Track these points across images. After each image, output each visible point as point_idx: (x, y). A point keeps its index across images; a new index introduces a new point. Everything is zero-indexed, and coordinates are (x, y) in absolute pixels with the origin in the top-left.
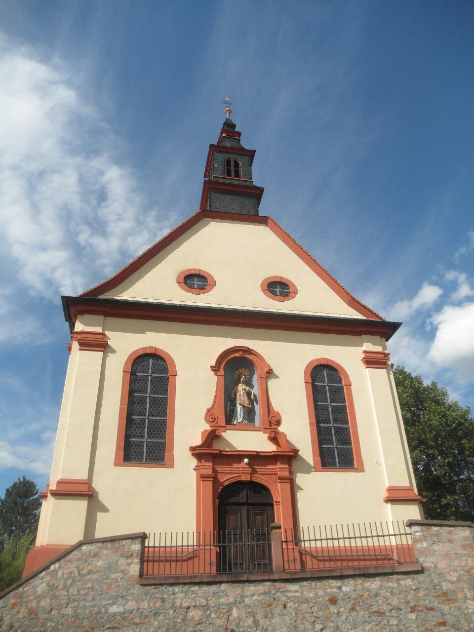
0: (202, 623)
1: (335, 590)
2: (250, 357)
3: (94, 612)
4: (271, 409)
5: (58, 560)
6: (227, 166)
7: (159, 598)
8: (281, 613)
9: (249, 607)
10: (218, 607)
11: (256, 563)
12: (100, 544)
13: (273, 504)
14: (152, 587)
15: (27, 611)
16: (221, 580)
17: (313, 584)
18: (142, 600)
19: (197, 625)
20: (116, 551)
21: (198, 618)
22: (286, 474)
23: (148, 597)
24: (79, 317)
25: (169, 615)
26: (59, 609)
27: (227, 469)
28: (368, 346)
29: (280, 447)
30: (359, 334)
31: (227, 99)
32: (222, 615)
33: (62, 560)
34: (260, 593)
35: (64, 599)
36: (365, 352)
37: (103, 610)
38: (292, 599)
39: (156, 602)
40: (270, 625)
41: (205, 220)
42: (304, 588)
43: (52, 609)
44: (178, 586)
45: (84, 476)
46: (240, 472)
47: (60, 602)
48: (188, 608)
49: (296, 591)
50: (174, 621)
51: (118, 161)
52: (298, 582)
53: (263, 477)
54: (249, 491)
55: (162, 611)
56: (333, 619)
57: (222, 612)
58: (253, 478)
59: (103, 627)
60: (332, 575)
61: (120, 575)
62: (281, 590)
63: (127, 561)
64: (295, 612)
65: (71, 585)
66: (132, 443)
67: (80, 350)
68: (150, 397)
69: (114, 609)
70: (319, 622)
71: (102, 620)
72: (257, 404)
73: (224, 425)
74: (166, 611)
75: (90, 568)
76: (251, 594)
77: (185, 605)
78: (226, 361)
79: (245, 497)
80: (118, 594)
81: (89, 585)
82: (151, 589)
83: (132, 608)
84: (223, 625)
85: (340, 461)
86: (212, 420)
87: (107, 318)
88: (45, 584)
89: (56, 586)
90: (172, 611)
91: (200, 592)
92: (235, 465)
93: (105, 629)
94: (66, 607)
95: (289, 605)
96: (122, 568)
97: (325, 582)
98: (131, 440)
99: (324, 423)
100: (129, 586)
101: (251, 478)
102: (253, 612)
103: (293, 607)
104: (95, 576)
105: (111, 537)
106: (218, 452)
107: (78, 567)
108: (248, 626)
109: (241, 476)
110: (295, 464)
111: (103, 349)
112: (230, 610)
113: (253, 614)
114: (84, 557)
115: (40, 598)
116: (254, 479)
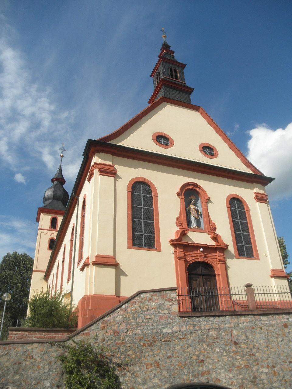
0: (218, 338)
1: (286, 320)
2: (197, 189)
3: (154, 332)
4: (210, 221)
5: (127, 302)
6: (170, 72)
7: (192, 324)
8: (260, 332)
9: (243, 329)
10: (226, 330)
11: (209, 308)
12: (152, 293)
13: (215, 275)
14: (187, 318)
15: (112, 331)
16: (226, 314)
17: (274, 317)
18: (182, 326)
19: (215, 339)
20: (162, 297)
21: (215, 335)
22: (222, 258)
23: (185, 324)
24: (96, 154)
25: (198, 334)
26: (133, 331)
27: (191, 254)
28: (256, 190)
29: (219, 243)
30: (252, 182)
31: (163, 29)
32: (228, 333)
33: (129, 302)
34: (247, 321)
35: (134, 325)
36: (255, 193)
37: (159, 331)
38: (264, 325)
39: (190, 326)
40: (254, 339)
41: (164, 103)
42: (270, 319)
43: (127, 331)
44: (202, 318)
45: (111, 254)
46: (197, 256)
47: (132, 327)
48: (209, 330)
49: (266, 321)
50: (202, 337)
51: (12, 45)
52: (267, 316)
53: (210, 260)
54: (202, 267)
55: (194, 332)
56: (286, 336)
57: (228, 332)
59: (161, 340)
60: (284, 312)
61: (167, 311)
62: (258, 320)
63: (170, 303)
64: (267, 332)
65: (137, 317)
66: (135, 235)
68: (143, 208)
69: (166, 331)
70: (280, 337)
71: (160, 337)
72: (201, 217)
73: (187, 228)
74: (196, 331)
75: (147, 307)
76: (243, 322)
77: (207, 328)
78: (184, 191)
79: (201, 271)
80: (167, 322)
81: (149, 317)
82: (187, 319)
83: (177, 330)
84: (230, 339)
85: (247, 253)
86: (180, 225)
88: (121, 316)
89: (128, 317)
90: (200, 331)
91: (214, 321)
92: (195, 252)
93: (162, 342)
94: (136, 329)
95: (263, 328)
96: (168, 307)
97: (281, 316)
98: (135, 233)
99: (237, 231)
100: (173, 318)
101: (204, 260)
102: (244, 332)
103: (265, 329)
104: (151, 312)
105: (158, 289)
106: (187, 243)
107: (140, 307)
108: (243, 339)
109: (199, 258)
110: (226, 253)
111: (114, 176)
112: (232, 331)
113: (244, 333)
114: (143, 300)
115: (120, 323)
116: (206, 261)
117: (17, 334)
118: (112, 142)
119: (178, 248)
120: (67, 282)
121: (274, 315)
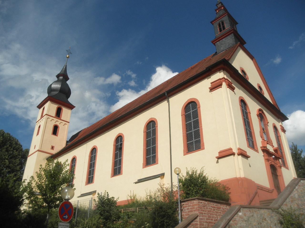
117: (201, 203)
119: (266, 153)
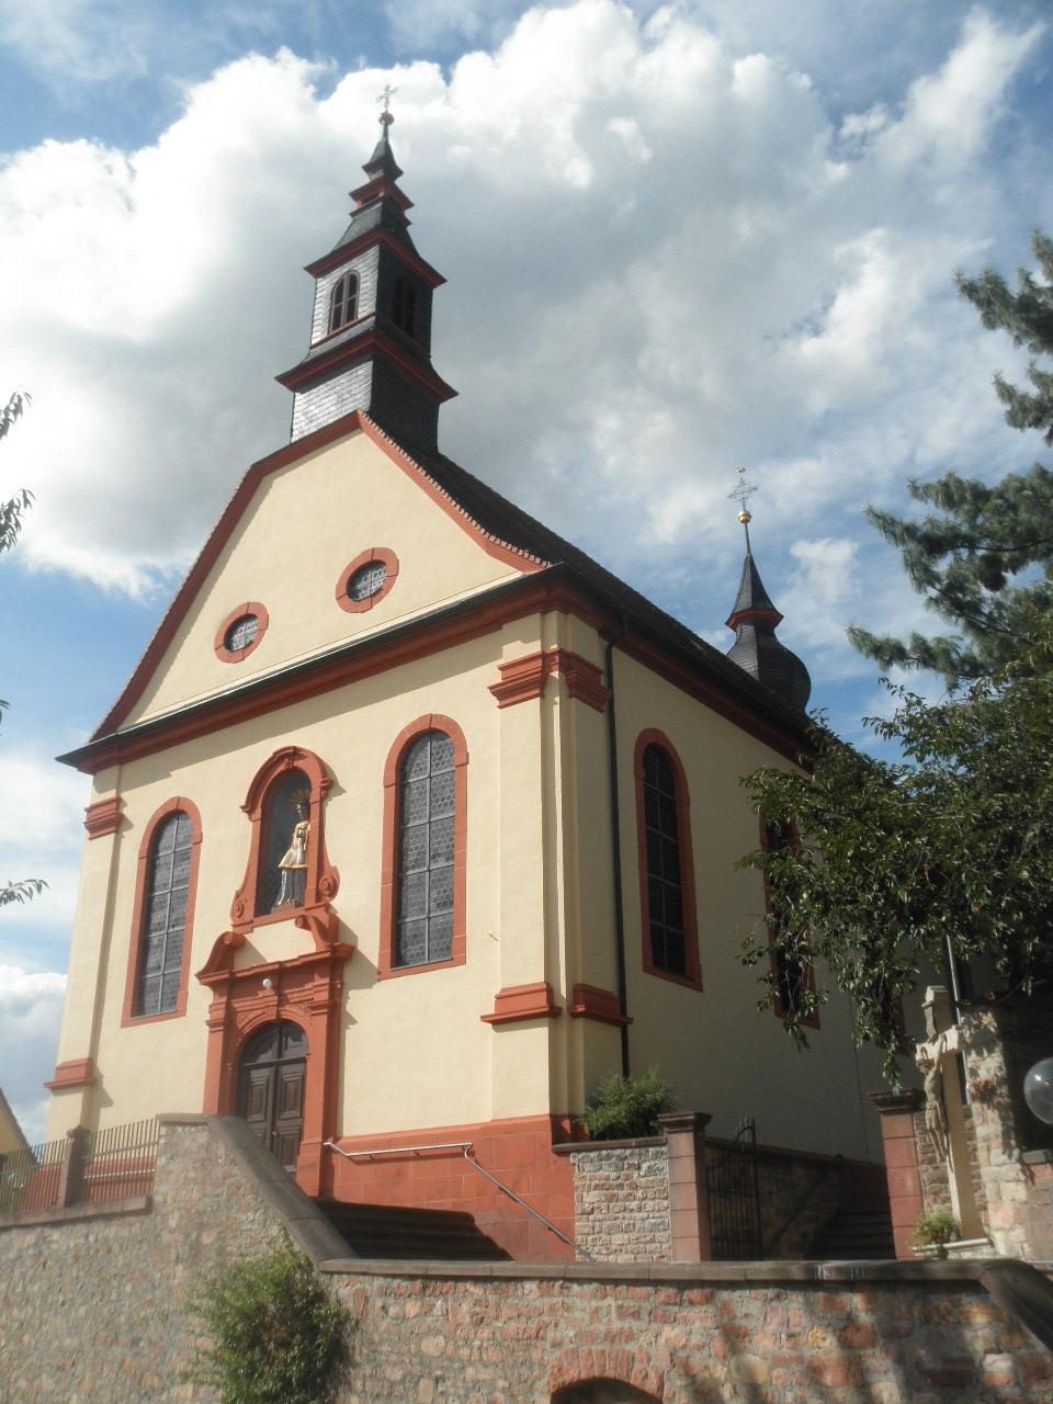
41: (266, 479)
58: (282, 1013)
67: (500, 707)
87: (548, 614)
118: (124, 729)
120: (308, 1080)
121: (93, 1223)
